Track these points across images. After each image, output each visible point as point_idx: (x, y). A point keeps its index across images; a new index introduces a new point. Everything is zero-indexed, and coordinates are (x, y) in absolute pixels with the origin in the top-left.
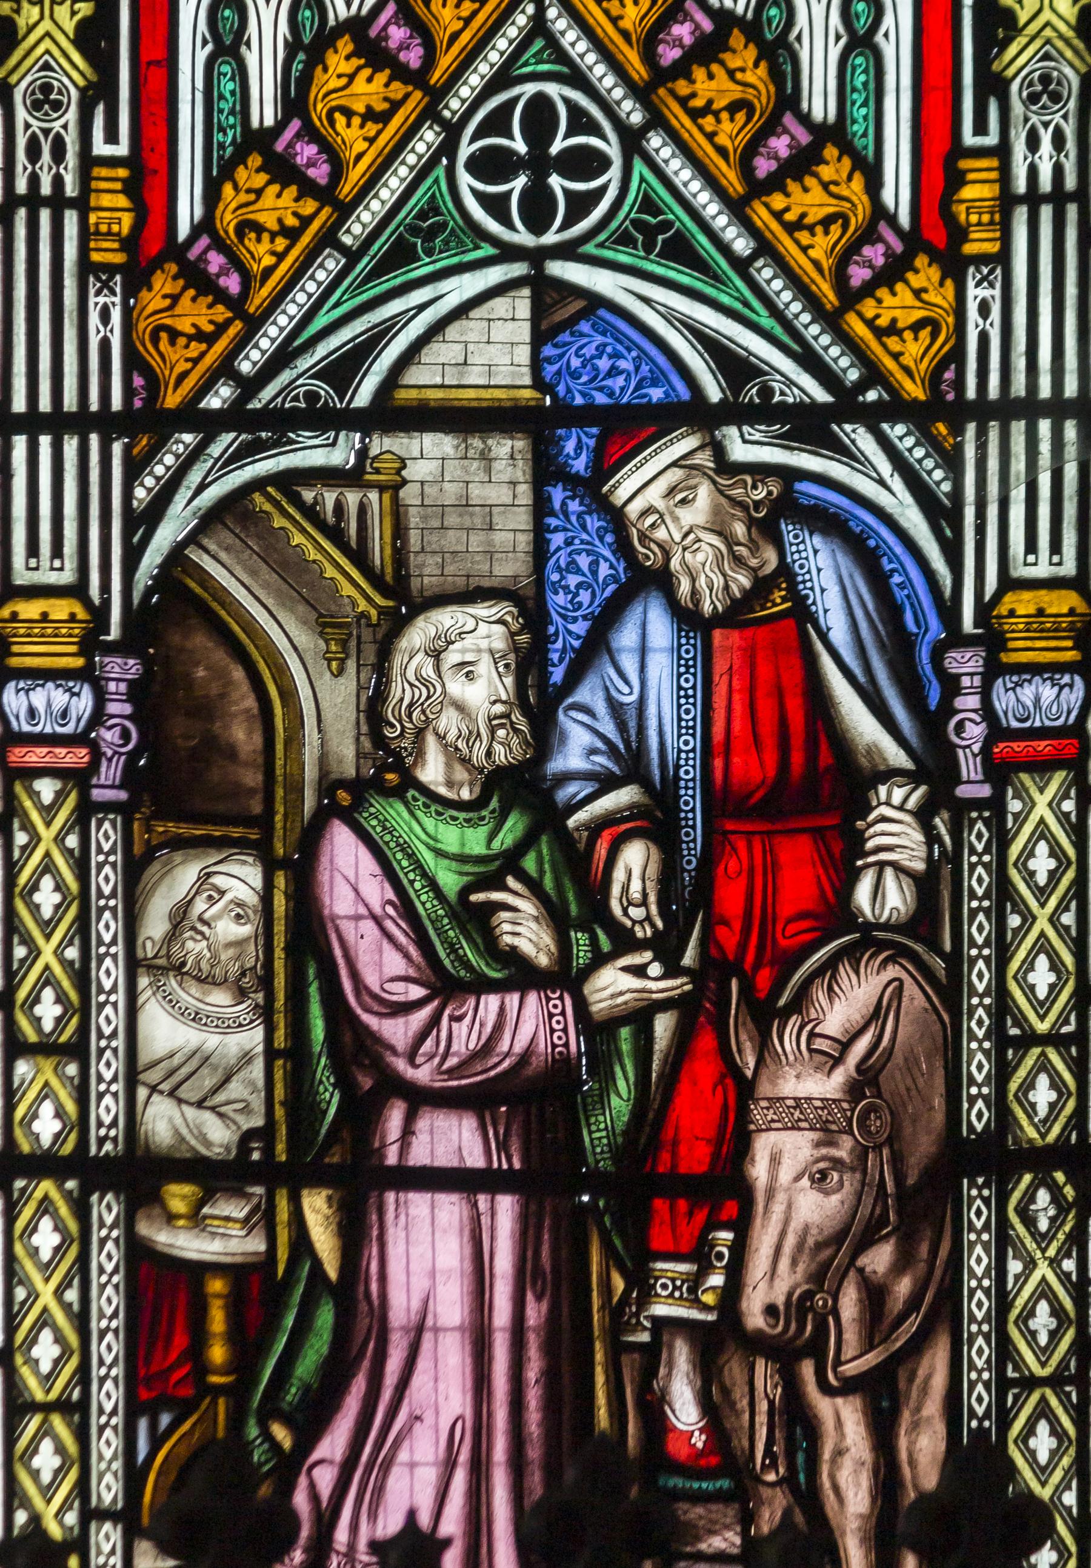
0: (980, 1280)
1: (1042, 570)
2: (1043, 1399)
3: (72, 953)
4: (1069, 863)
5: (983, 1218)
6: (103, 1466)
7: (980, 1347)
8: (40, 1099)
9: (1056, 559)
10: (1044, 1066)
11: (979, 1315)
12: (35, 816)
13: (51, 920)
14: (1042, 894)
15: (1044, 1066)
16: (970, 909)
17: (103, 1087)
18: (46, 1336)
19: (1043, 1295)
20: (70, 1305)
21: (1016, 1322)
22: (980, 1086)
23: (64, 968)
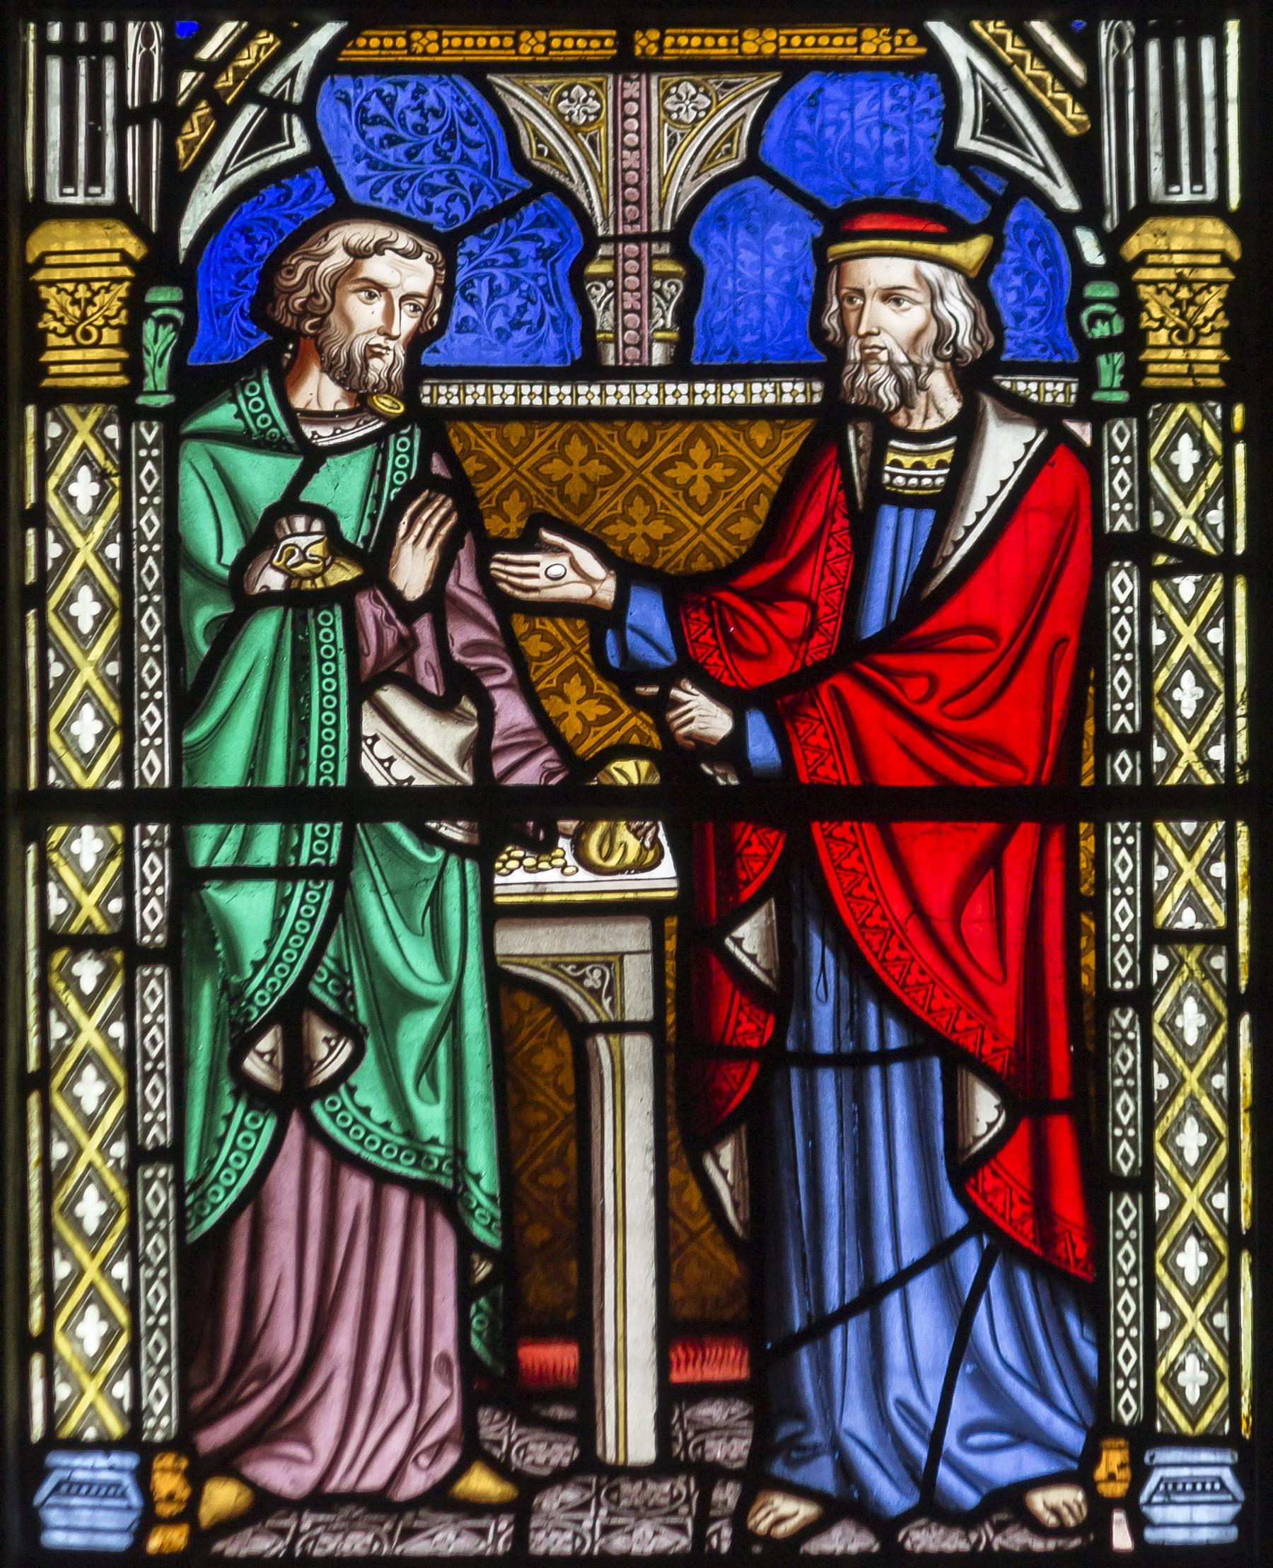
0: (1127, 1330)
1: (1185, 194)
2: (1193, 1423)
3: (113, 551)
4: (1222, 1378)
5: (1128, 967)
6: (162, 1224)
7: (1123, 919)
8: (85, 1302)
9: (1198, 188)
10: (1193, 1415)
11: (1126, 1296)
12: (73, 1006)
13: (92, 872)
14: (1193, 1297)
15: (1186, 426)
16: (1110, 465)
17: (158, 741)
18: (91, 1225)
19: (1188, 666)
20: (119, 1282)
21: (1162, 1141)
22: (1122, 455)
23: (105, 685)
